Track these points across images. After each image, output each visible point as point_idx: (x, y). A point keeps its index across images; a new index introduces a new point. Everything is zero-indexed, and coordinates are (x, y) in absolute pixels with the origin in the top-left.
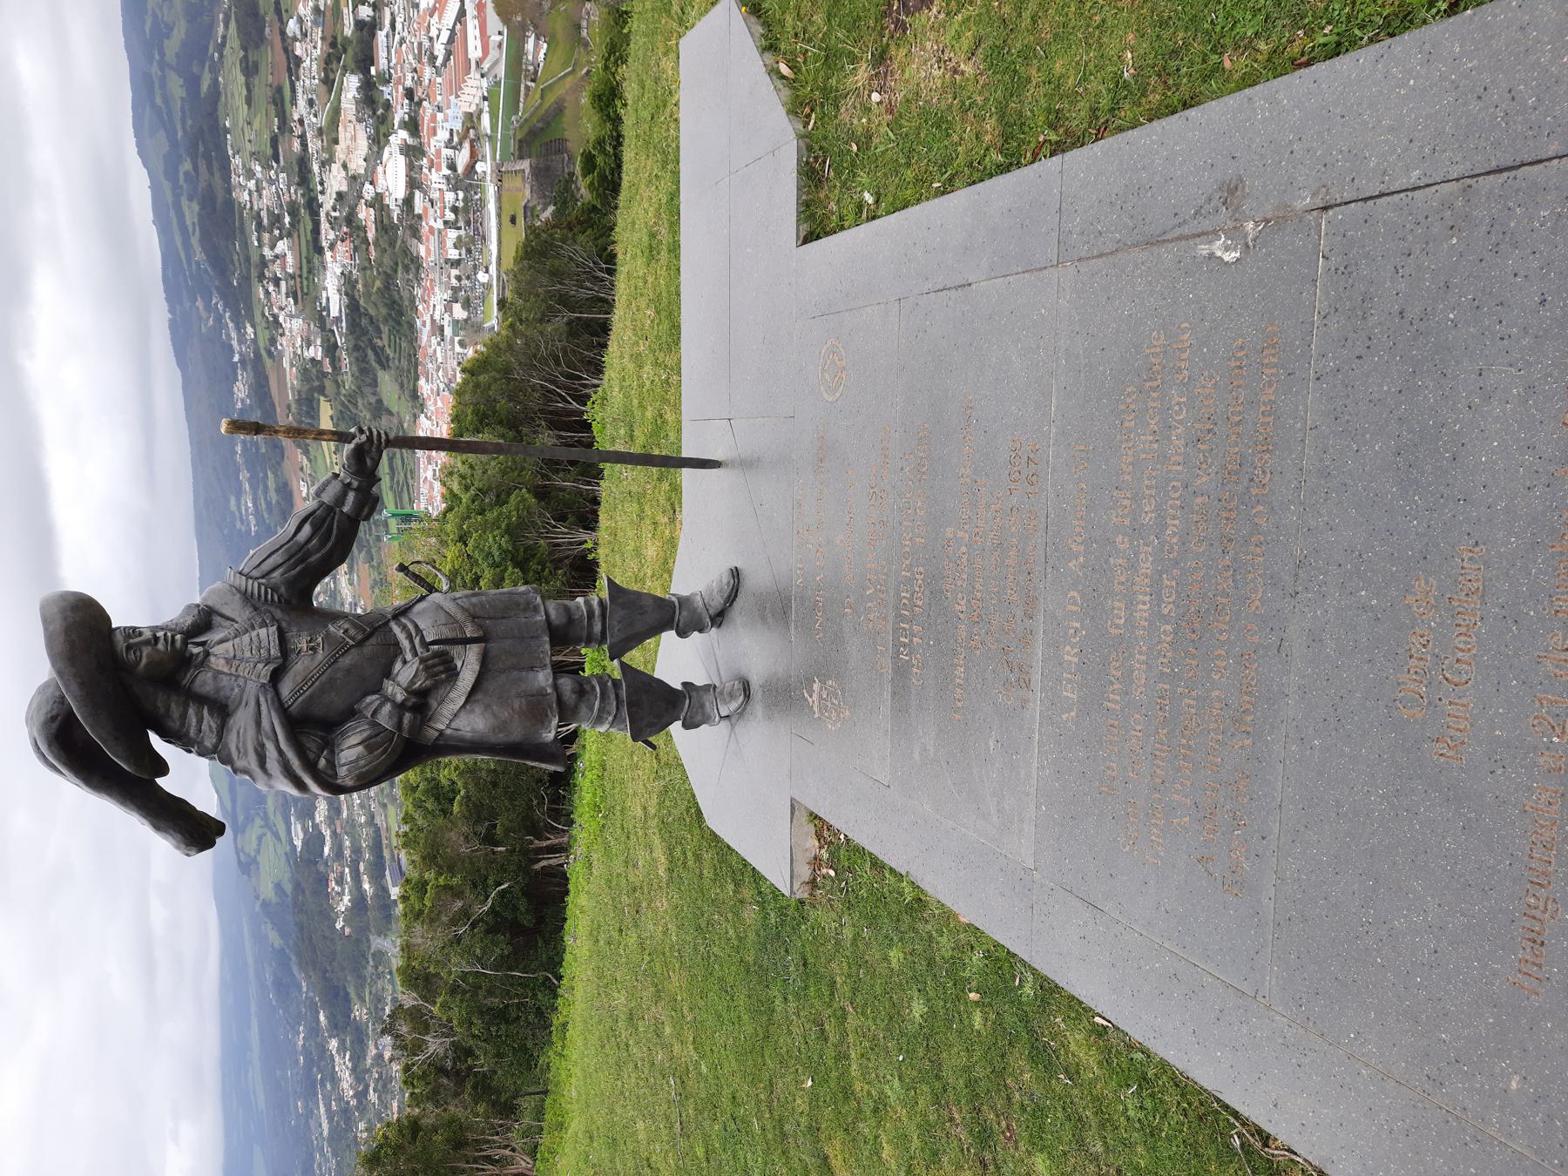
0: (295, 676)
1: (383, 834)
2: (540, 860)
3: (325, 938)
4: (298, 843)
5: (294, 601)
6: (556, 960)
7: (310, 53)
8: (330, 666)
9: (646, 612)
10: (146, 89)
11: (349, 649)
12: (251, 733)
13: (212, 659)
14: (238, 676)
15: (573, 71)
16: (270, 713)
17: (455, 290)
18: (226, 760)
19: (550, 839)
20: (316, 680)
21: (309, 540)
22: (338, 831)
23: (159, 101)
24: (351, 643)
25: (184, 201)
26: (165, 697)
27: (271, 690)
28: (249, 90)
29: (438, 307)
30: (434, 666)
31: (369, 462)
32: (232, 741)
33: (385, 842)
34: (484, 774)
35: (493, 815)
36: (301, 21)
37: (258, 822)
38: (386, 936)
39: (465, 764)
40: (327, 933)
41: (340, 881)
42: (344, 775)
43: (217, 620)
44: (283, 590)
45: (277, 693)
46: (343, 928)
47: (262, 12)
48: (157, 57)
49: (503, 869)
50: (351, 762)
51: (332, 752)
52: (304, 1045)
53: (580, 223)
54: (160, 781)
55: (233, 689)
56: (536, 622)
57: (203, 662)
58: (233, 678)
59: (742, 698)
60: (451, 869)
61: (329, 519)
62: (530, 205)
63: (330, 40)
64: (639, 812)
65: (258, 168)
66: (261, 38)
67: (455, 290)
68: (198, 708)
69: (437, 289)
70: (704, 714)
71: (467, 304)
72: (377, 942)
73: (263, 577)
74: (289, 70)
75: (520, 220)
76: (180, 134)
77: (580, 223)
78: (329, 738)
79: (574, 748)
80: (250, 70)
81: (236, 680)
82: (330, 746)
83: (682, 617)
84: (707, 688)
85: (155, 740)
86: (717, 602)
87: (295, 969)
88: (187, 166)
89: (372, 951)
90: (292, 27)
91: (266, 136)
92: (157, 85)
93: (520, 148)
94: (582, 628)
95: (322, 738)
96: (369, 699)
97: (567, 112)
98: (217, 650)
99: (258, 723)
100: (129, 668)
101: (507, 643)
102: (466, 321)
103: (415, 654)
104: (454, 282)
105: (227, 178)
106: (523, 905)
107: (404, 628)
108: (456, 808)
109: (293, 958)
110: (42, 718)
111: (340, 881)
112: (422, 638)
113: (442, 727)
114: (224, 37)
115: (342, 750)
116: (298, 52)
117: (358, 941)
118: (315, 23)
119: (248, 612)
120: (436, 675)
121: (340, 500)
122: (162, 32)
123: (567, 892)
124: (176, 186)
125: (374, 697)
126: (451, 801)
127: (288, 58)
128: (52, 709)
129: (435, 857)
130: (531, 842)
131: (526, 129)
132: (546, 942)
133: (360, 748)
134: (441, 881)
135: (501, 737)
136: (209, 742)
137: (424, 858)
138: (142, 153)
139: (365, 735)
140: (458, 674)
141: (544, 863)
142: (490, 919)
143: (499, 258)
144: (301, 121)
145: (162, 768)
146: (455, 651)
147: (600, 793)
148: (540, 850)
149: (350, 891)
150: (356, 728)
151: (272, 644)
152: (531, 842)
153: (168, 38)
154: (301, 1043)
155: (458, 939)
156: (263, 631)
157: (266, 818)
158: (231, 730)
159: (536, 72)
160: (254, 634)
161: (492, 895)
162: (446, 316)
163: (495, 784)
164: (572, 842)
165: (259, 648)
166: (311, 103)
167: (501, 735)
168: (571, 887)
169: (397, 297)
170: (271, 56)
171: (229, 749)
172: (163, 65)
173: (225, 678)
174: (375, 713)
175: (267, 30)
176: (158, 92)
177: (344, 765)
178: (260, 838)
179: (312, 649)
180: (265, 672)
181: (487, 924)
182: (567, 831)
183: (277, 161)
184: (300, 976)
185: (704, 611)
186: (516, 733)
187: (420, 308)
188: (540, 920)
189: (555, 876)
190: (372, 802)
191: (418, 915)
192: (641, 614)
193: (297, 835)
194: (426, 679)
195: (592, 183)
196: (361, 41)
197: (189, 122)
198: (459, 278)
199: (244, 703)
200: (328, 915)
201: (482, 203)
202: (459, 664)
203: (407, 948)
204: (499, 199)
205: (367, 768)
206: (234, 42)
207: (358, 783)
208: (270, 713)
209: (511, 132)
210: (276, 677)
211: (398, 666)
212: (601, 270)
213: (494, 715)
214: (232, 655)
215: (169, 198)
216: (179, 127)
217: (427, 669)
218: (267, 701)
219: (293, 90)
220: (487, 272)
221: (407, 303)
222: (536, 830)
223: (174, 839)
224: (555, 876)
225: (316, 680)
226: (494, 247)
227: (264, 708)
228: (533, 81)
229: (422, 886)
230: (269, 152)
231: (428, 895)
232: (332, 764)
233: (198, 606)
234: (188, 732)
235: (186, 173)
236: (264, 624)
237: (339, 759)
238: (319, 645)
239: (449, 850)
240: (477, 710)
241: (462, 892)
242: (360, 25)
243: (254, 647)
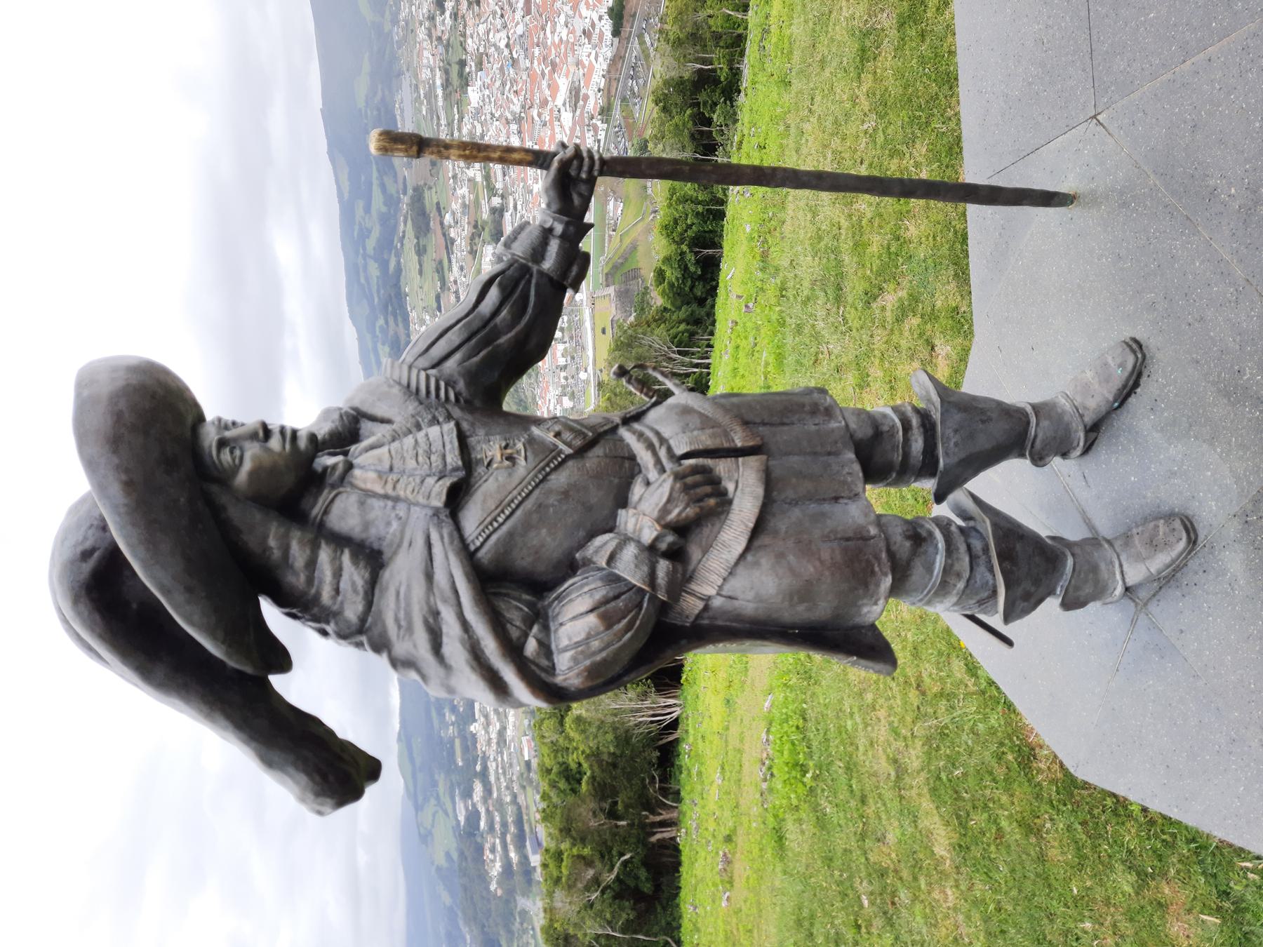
0: (484, 501)
1: (524, 811)
2: (654, 833)
3: (482, 898)
4: (462, 818)
5: (478, 403)
6: (674, 924)
7: (460, 235)
8: (537, 486)
9: (990, 419)
10: (354, 273)
11: (564, 461)
12: (418, 590)
13: (357, 472)
14: (396, 499)
15: (643, 219)
16: (447, 558)
17: (564, 387)
18: (381, 645)
19: (661, 814)
20: (518, 506)
21: (496, 312)
22: (491, 808)
23: (363, 280)
24: (568, 451)
25: (379, 346)
26: (282, 530)
27: (450, 520)
28: (421, 265)
29: (552, 401)
30: (696, 485)
31: (577, 200)
32: (388, 607)
33: (525, 817)
34: (605, 757)
35: (615, 793)
36: (453, 213)
37: (433, 801)
38: (528, 897)
39: (590, 748)
40: (484, 893)
41: (493, 850)
42: (567, 669)
43: (366, 426)
44: (461, 385)
45: (458, 527)
46: (496, 890)
47: (428, 211)
48: (361, 251)
49: (625, 841)
50: (578, 644)
51: (546, 628)
53: (655, 321)
54: (276, 681)
55: (389, 524)
56: (833, 430)
57: (342, 478)
58: (390, 503)
59: (1182, 544)
60: (583, 840)
61: (523, 283)
62: (616, 319)
63: (473, 223)
64: (884, 767)
65: (428, 317)
66: (428, 229)
67: (564, 387)
68: (335, 551)
69: (551, 388)
70: (1097, 582)
71: (572, 396)
72: (522, 902)
73: (433, 367)
74: (447, 248)
75: (609, 331)
76: (376, 300)
77: (655, 321)
78: (539, 605)
79: (678, 734)
80: (421, 251)
81: (394, 508)
82: (539, 617)
83: (1038, 430)
84: (1085, 541)
85: (271, 613)
86: (1097, 398)
87: (461, 923)
88: (381, 321)
89: (518, 909)
90: (448, 218)
91: (433, 296)
92: (361, 270)
93: (607, 280)
94: (895, 447)
95: (531, 605)
96: (599, 541)
97: (640, 248)
99: (429, 576)
100: (223, 478)
101: (795, 460)
102: (572, 408)
103: (663, 470)
104: (563, 381)
105: (407, 327)
106: (643, 874)
107: (640, 436)
108: (584, 787)
109: (460, 914)
110: (68, 553)
111: (493, 850)
112: (669, 449)
113: (710, 591)
114: (404, 232)
115: (561, 624)
116: (452, 235)
117: (507, 902)
118: (463, 213)
119: (412, 407)
120: (700, 500)
121: (538, 252)
122: (365, 234)
123: (679, 864)
124: (374, 336)
125: (607, 536)
126: (579, 782)
127: (446, 240)
128: (85, 538)
129: (570, 830)
130: (647, 817)
131: (610, 265)
132: (664, 909)
133: (592, 619)
134: (575, 851)
135: (800, 613)
136: (352, 611)
137: (561, 831)
138: (352, 317)
139: (598, 596)
140: (730, 502)
141: (658, 836)
142: (616, 886)
143: (595, 360)
144: (455, 282)
145: (280, 659)
146: (721, 467)
147: (802, 747)
148: (654, 825)
149: (501, 859)
150: (582, 586)
151: (448, 447)
152: (647, 817)
153: (368, 237)
155: (591, 905)
156: (434, 431)
157: (438, 798)
158: (387, 588)
159: (616, 224)
160: (420, 435)
161: (618, 865)
162: (558, 407)
163: (615, 766)
164: (681, 817)
165: (429, 454)
166: (462, 268)
167: (801, 608)
168: (684, 858)
169: (523, 397)
170: (435, 240)
171: (384, 626)
172: (365, 256)
173: (377, 503)
174: (611, 559)
175: (432, 223)
176: (362, 275)
177: (565, 650)
178: (434, 815)
179: (510, 458)
180: (438, 492)
181: (614, 891)
182: (677, 807)
183: (440, 311)
184: (465, 930)
185: (1077, 419)
186: (822, 609)
187: (540, 403)
188: (658, 888)
189: (667, 848)
190: (514, 785)
191: (557, 881)
192: (983, 422)
193: (460, 812)
194: (687, 505)
195: (664, 291)
196: (494, 221)
197: (382, 292)
198: (566, 378)
199: (406, 544)
200: (483, 878)
201: (581, 322)
202: (730, 487)
203: (550, 910)
204: (593, 317)
205: (604, 654)
206: (410, 233)
207: (589, 684)
208: (447, 558)
209: (600, 269)
210: (457, 496)
211: (637, 490)
212: (674, 352)
213: (792, 570)
214: (387, 466)
215: (370, 345)
216: (375, 295)
217: (687, 488)
218: (442, 538)
219: (450, 261)
220: (586, 371)
221: (530, 400)
222: (652, 807)
223: (297, 783)
224: (667, 848)
225: (518, 506)
226: (590, 353)
228: (614, 230)
229: (558, 856)
230: (435, 305)
231: (564, 864)
232: (545, 648)
233: (340, 409)
234: (318, 596)
235: (381, 327)
236: (434, 421)
237: (557, 639)
239: (580, 824)
240: (763, 561)
241: (592, 862)
242: (493, 211)
243: (420, 451)
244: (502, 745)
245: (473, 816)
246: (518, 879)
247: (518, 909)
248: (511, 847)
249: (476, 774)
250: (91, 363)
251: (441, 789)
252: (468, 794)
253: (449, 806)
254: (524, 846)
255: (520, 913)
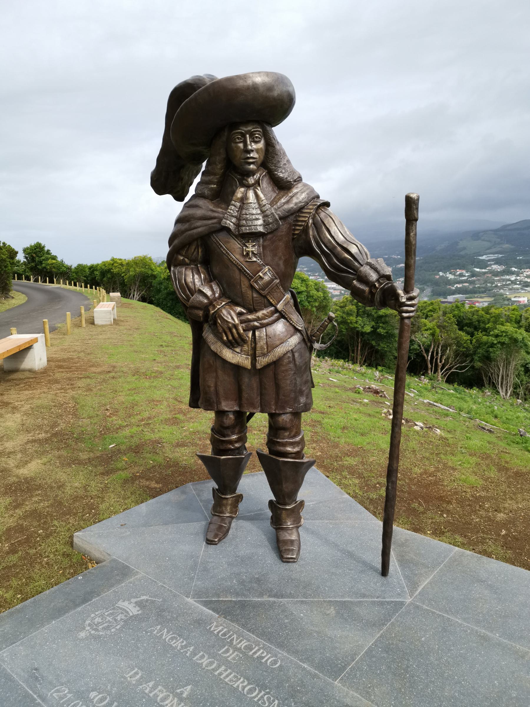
52: (392, 257)
89: (425, 287)
98: (251, 194)
154: (393, 256)
156: (260, 222)
218: (213, 224)
227: (210, 222)
236: (266, 224)
238: (250, 258)
244: (525, 284)
245: (483, 264)
247: (425, 287)
250: (287, 78)
251: (506, 246)
252: (498, 262)
253: (494, 250)
255: (424, 287)
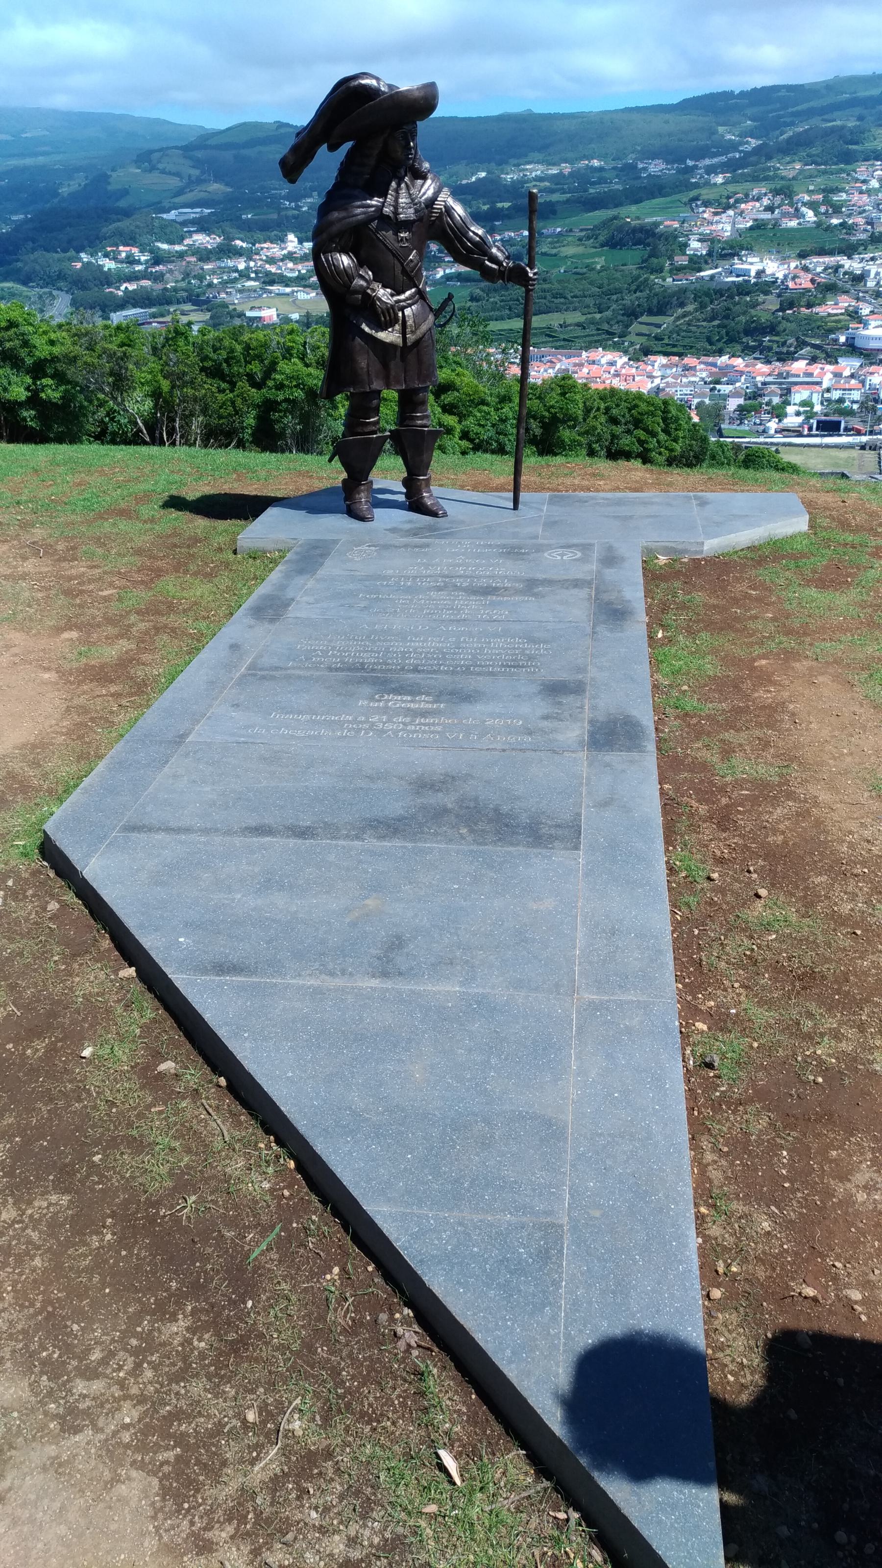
54: (325, 146)
85: (349, 145)
145: (333, 148)
157: (199, 181)
236: (416, 211)
246: (92, 294)
248: (132, 287)
249: (229, 239)
252: (203, 226)
253: (189, 197)
254: (135, 306)
255: (51, 294)
